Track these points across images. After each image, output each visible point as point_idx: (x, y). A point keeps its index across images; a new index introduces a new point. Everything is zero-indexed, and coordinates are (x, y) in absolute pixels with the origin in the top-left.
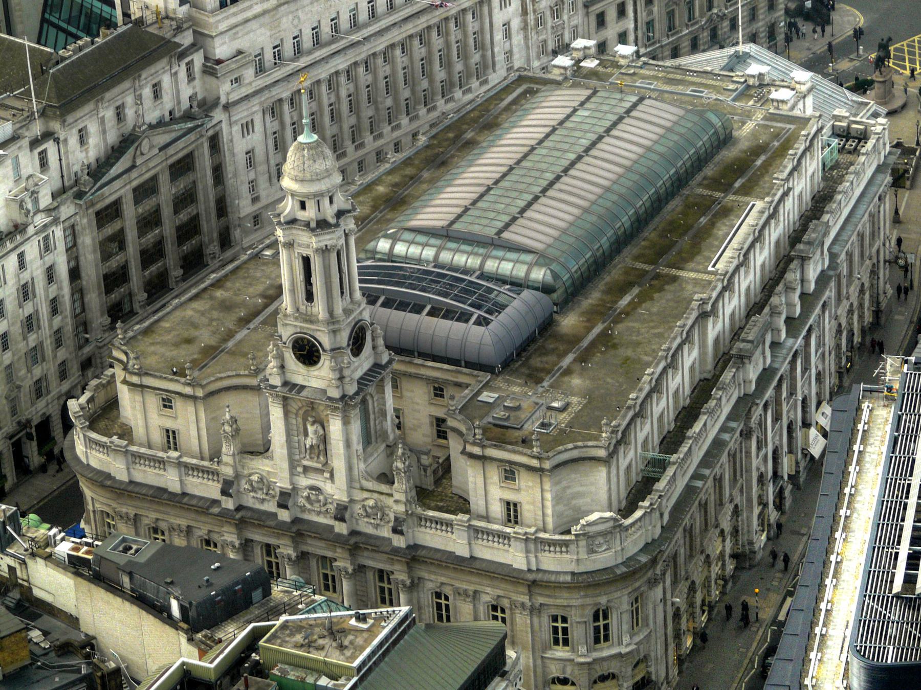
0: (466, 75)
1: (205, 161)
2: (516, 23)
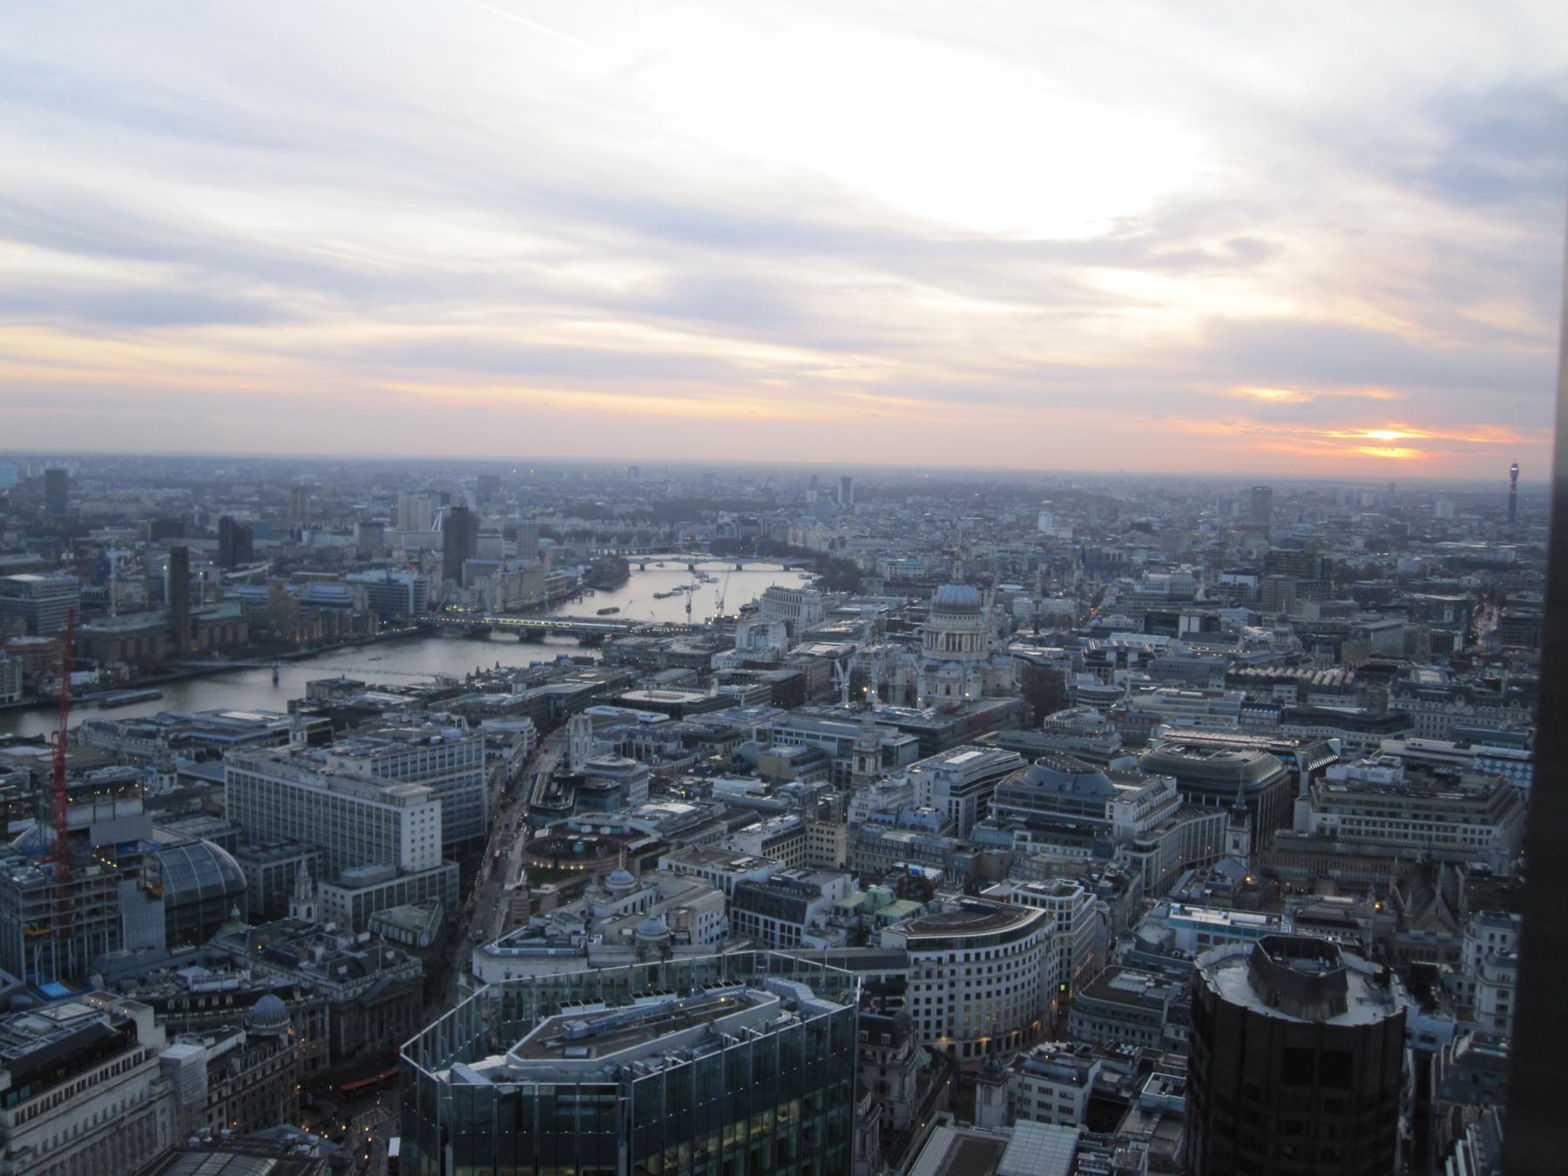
0: (142, 1151)
2: (168, 1124)
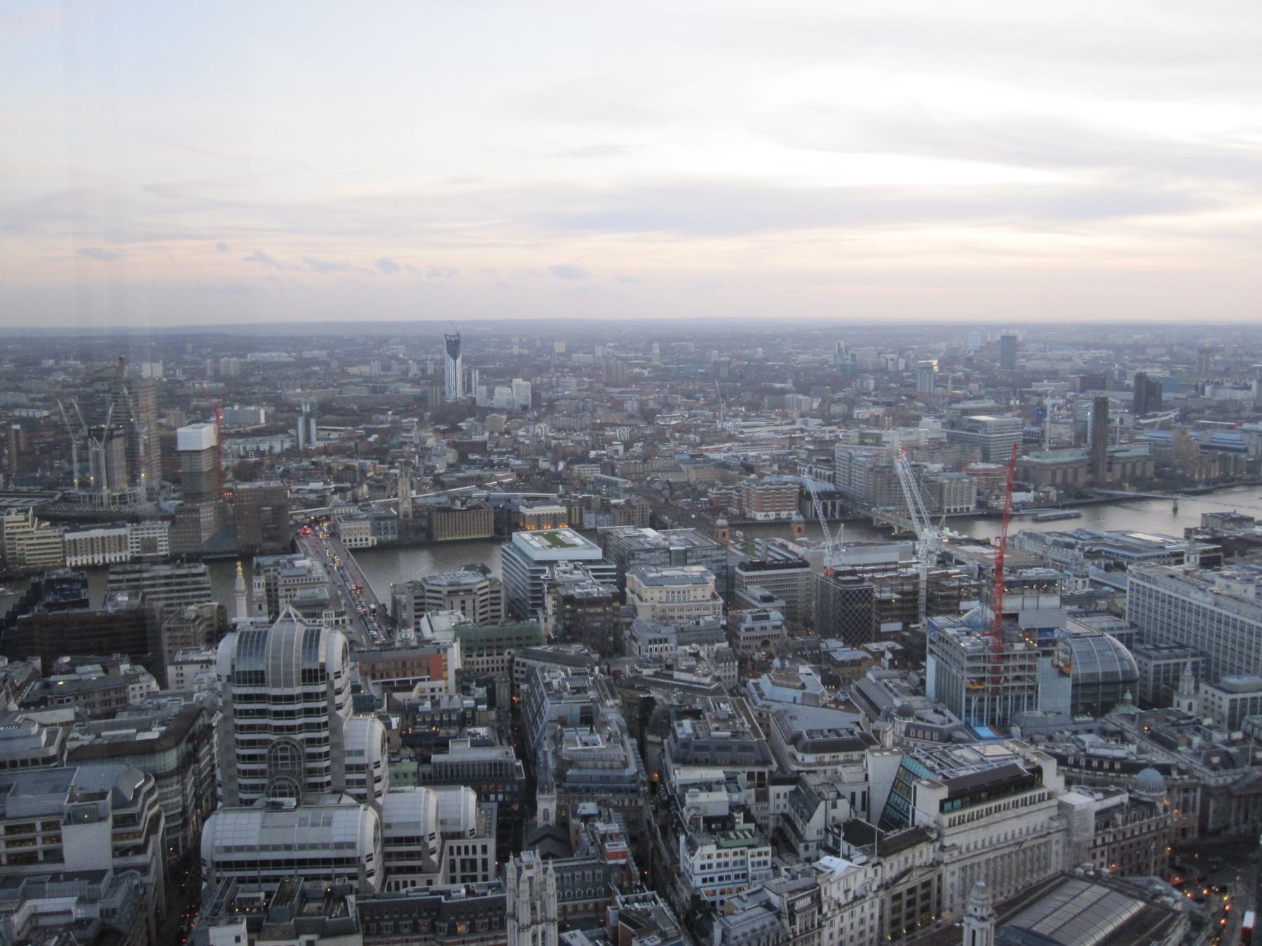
1: (935, 884)
